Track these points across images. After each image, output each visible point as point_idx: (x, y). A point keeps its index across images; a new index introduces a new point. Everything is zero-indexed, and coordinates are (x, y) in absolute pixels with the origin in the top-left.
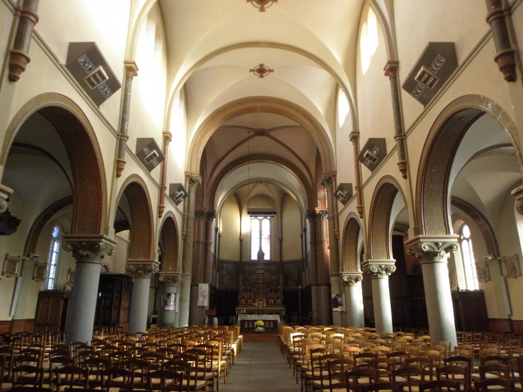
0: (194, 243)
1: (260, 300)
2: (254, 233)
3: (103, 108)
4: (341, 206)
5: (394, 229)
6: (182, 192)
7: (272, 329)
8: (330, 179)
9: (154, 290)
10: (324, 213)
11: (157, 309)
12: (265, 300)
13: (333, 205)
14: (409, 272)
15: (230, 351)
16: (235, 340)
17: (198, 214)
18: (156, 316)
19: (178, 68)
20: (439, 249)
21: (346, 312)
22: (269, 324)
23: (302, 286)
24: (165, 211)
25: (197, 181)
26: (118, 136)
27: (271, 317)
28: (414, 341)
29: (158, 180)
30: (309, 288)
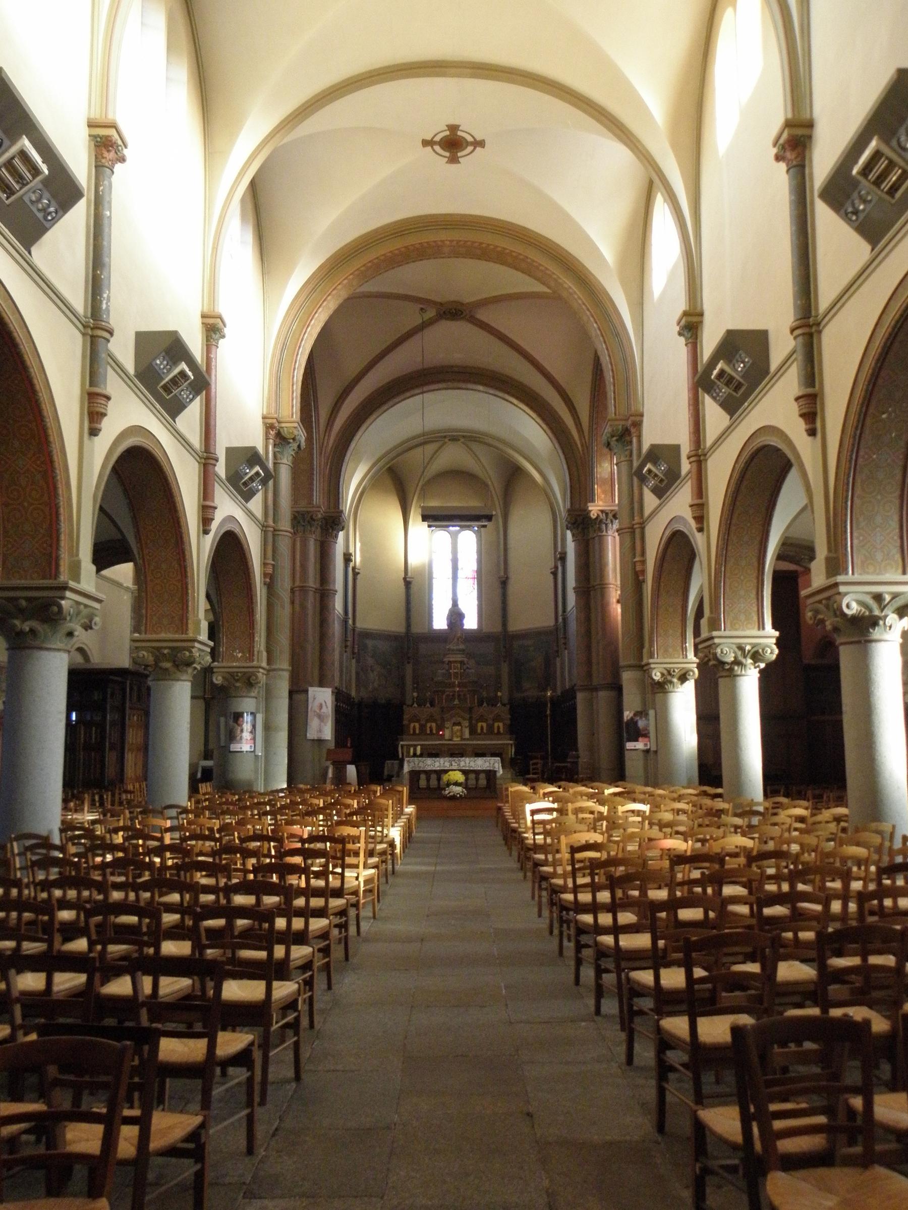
0: (292, 591)
1: (455, 724)
2: (437, 567)
3: (40, 254)
4: (650, 500)
5: (780, 557)
6: (257, 468)
7: (485, 789)
8: (627, 433)
9: (201, 704)
10: (610, 516)
11: (211, 746)
12: (466, 723)
13: (632, 499)
14: (808, 656)
15: (385, 846)
16: (396, 818)
17: (301, 520)
18: (209, 763)
19: (233, 136)
20: (882, 610)
21: (656, 752)
22: (477, 779)
23: (554, 690)
24: (219, 517)
25: (294, 439)
26: (84, 327)
27: (480, 764)
28: (811, 820)
29: (196, 440)
30: (569, 695)
